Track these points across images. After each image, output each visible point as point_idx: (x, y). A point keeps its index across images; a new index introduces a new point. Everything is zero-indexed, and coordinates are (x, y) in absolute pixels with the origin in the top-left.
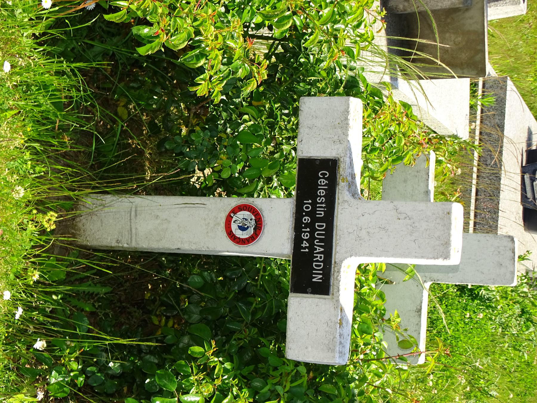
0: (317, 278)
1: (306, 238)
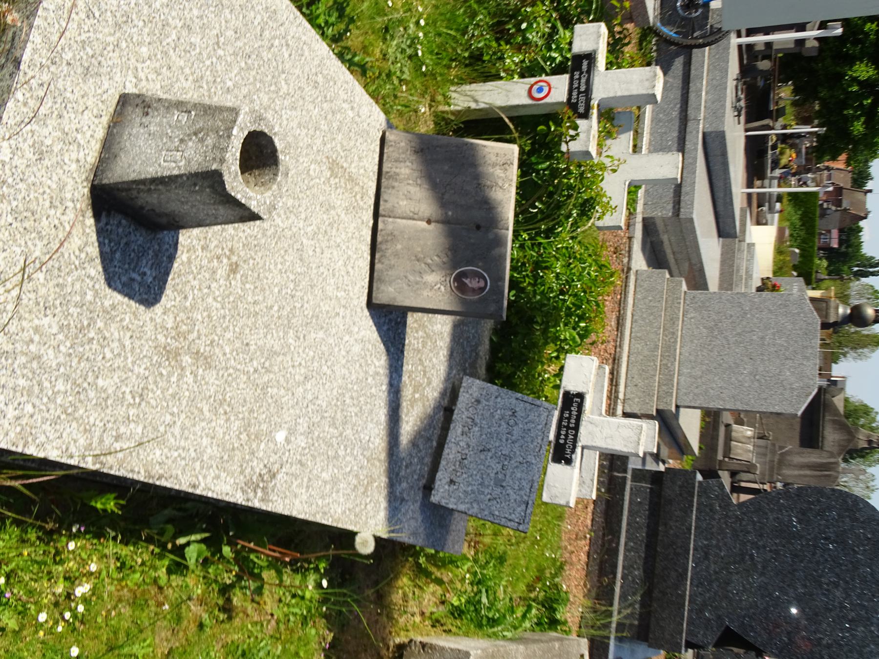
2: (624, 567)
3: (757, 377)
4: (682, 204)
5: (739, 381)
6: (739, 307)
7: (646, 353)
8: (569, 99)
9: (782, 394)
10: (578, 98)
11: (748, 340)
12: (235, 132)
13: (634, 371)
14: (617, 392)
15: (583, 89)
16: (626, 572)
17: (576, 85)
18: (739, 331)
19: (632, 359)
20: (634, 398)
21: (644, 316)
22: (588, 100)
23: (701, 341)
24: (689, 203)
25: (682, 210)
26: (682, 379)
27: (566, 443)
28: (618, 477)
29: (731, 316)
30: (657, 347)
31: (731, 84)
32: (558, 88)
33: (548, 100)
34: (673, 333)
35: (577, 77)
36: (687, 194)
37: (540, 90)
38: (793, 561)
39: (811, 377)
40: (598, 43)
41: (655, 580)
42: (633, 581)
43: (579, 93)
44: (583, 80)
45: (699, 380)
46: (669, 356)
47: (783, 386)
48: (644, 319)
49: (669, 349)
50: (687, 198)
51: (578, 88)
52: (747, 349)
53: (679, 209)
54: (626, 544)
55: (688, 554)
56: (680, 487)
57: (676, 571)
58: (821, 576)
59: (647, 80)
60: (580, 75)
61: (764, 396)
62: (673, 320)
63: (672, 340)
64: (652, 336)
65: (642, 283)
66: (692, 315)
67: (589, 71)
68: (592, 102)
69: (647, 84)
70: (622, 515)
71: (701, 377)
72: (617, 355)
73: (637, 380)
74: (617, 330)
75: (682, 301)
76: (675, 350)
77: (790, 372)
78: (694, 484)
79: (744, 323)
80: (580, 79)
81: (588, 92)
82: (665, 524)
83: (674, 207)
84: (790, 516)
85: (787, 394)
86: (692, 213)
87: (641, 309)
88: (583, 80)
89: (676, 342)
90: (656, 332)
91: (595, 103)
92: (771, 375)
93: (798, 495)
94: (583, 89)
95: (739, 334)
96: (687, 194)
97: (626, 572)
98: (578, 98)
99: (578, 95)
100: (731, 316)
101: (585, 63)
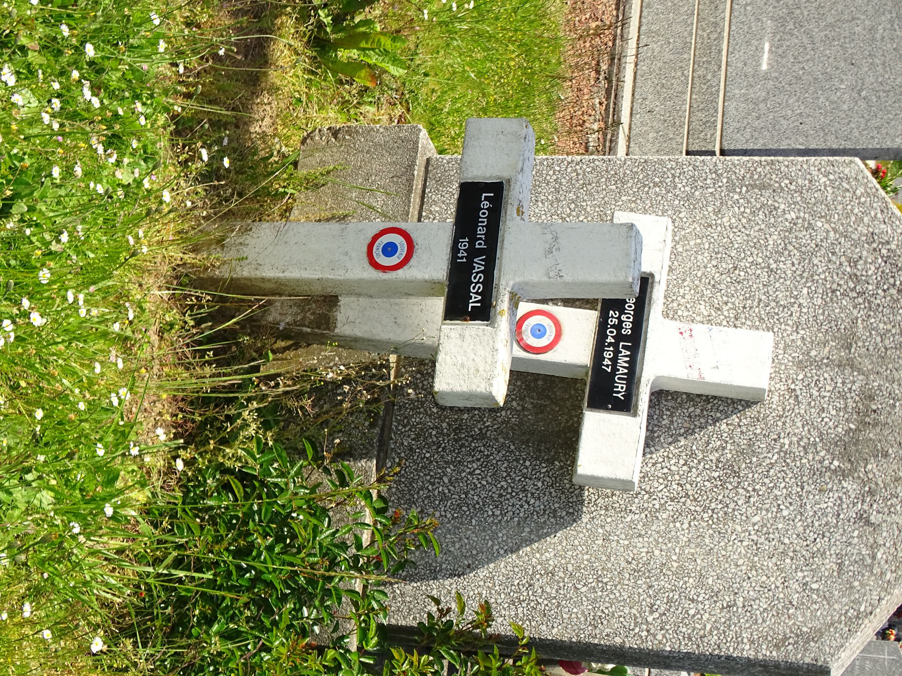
3: (863, 94)
5: (832, 103)
7: (668, 56)
11: (847, 34)
12: (416, 173)
13: (646, 88)
14: (617, 111)
18: (830, 19)
19: (643, 67)
22: (632, 378)
26: (732, 106)
27: (615, 369)
30: (686, 45)
31: (630, 60)
34: (716, 25)
37: (539, 332)
45: (762, 105)
46: (709, 62)
49: (710, 49)
52: (845, 50)
61: (875, 123)
64: (679, 28)
71: (765, 100)
72: (618, 50)
73: (652, 102)
74: (617, 9)
76: (720, 51)
89: (720, 38)
92: (887, 88)
95: (831, 25)
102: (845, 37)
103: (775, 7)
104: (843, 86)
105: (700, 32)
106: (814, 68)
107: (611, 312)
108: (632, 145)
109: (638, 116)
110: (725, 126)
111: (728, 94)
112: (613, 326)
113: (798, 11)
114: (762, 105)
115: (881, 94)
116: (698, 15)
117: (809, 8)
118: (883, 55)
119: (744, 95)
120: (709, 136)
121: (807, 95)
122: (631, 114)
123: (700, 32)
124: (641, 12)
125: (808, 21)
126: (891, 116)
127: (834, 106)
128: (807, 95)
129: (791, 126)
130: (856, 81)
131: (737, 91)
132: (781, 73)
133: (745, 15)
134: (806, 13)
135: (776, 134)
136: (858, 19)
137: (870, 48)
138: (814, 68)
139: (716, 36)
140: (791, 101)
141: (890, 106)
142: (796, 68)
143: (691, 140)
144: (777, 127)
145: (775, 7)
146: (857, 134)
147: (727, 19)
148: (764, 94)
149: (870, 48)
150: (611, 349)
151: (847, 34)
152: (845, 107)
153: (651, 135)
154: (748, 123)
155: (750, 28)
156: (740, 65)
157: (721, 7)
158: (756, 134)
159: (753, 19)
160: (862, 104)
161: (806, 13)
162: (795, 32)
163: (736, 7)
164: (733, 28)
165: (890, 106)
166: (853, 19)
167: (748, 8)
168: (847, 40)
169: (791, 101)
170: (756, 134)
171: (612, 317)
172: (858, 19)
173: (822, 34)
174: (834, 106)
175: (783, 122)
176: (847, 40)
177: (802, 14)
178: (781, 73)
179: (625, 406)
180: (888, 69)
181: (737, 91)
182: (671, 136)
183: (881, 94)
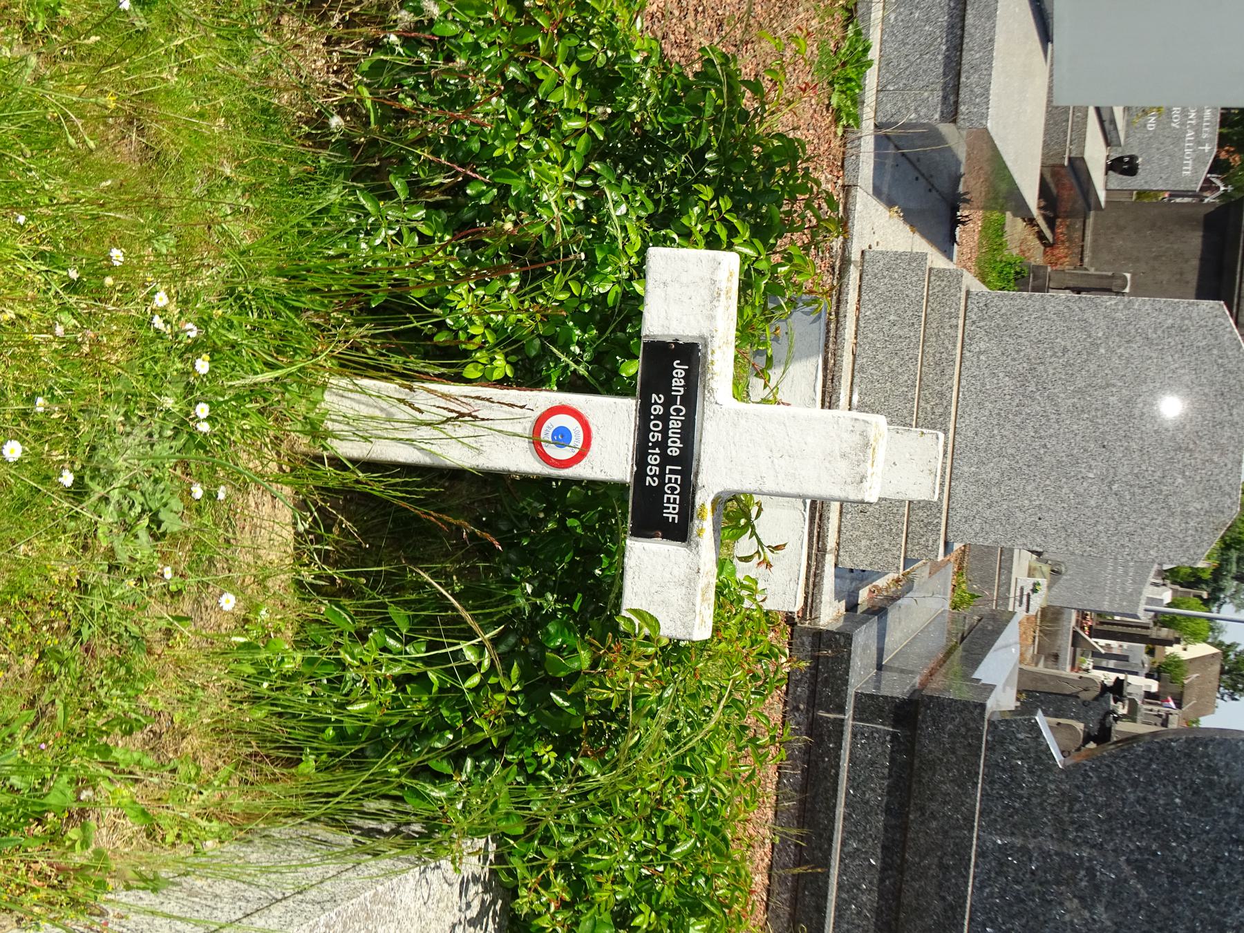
0: (671, 513)
1: (657, 407)
2: (840, 887)
3: (1115, 487)
4: (964, 94)
5: (1077, 495)
6: (1083, 329)
8: (640, 475)
9: (1165, 524)
10: (661, 476)
11: (1099, 405)
15: (674, 451)
16: (844, 896)
17: (656, 436)
18: (1080, 383)
20: (858, 539)
21: (880, 357)
22: (688, 491)
23: (1000, 404)
24: (978, 90)
25: (963, 108)
28: (827, 720)
29: (1065, 350)
32: (607, 434)
33: (581, 471)
34: (941, 395)
35: (658, 410)
36: (975, 68)
38: (1171, 883)
39: (1227, 489)
40: (712, 318)
41: (902, 916)
42: (859, 913)
43: (666, 460)
44: (675, 424)
45: (994, 490)
47: (1169, 508)
48: (879, 365)
50: (974, 78)
51: (663, 445)
53: (956, 103)
54: (844, 844)
55: (967, 868)
56: (951, 735)
57: (943, 898)
58: (1224, 914)
59: (843, 456)
60: (666, 405)
61: (1128, 527)
62: (941, 366)
63: (939, 410)
65: (875, 284)
66: (983, 346)
67: (690, 400)
68: (699, 500)
69: (843, 467)
70: (835, 796)
71: (999, 483)
75: (961, 322)
77: (1184, 476)
78: (979, 730)
79: (1093, 367)
80: (665, 418)
81: (686, 462)
82: (922, 810)
83: (945, 98)
84: (1169, 795)
85: (1176, 524)
86: (984, 116)
87: (872, 343)
88: (675, 424)
90: (904, 394)
91: (704, 498)
92: (1144, 483)
93: (1188, 755)
94: (674, 451)
96: (975, 68)
97: (844, 896)
98: (661, 476)
99: (662, 466)
100: (1065, 350)
101: (679, 371)
102: (1097, 409)
103: (1014, 360)
104: (1091, 475)
105: (922, 404)
106: (1058, 447)
107: (654, 396)
108: (841, 553)
109: (849, 516)
110: (952, 513)
111: (955, 471)
112: (657, 417)
113: (1042, 368)
114: (994, 490)
115: (1136, 489)
116: (921, 380)
117: (1055, 365)
118: (1141, 438)
119: (975, 474)
120: (931, 543)
121: (1048, 482)
122: (841, 513)
123: (922, 404)
124: (853, 376)
125: (1053, 383)
126: (1146, 521)
127: (1080, 499)
128: (1048, 482)
129: (1029, 520)
130: (1107, 470)
131: (966, 469)
132: (1018, 449)
133: (978, 366)
134: (1051, 371)
135: (1009, 528)
136: (1114, 385)
137: (1126, 428)
138: (1058, 447)
139: (941, 410)
140: (1029, 488)
141: (1146, 507)
142: (1036, 444)
143: (910, 546)
144: (1011, 521)
145: (1014, 360)
146: (1104, 540)
147: (955, 388)
148: (997, 475)
149: (1126, 428)
150: (657, 451)
151: (1099, 405)
152: (1093, 503)
153: (863, 542)
154: (978, 512)
155: (983, 385)
156: (970, 434)
157: (948, 371)
158: (987, 528)
159: (987, 372)
160: (1113, 501)
161: (1051, 371)
162: (1037, 395)
163: (968, 354)
164: (963, 383)
165: (1146, 507)
166: (1108, 385)
167: (982, 357)
168: (1099, 413)
169: (1029, 488)
170: (987, 528)
171: (656, 403)
172: (1114, 385)
173: (1069, 402)
174: (1080, 499)
175: (1019, 514)
176: (1099, 413)
177: (1046, 372)
178: (1018, 449)
179: (679, 532)
180: (1146, 457)
181: (966, 469)
182: (887, 546)
183: (1136, 489)
